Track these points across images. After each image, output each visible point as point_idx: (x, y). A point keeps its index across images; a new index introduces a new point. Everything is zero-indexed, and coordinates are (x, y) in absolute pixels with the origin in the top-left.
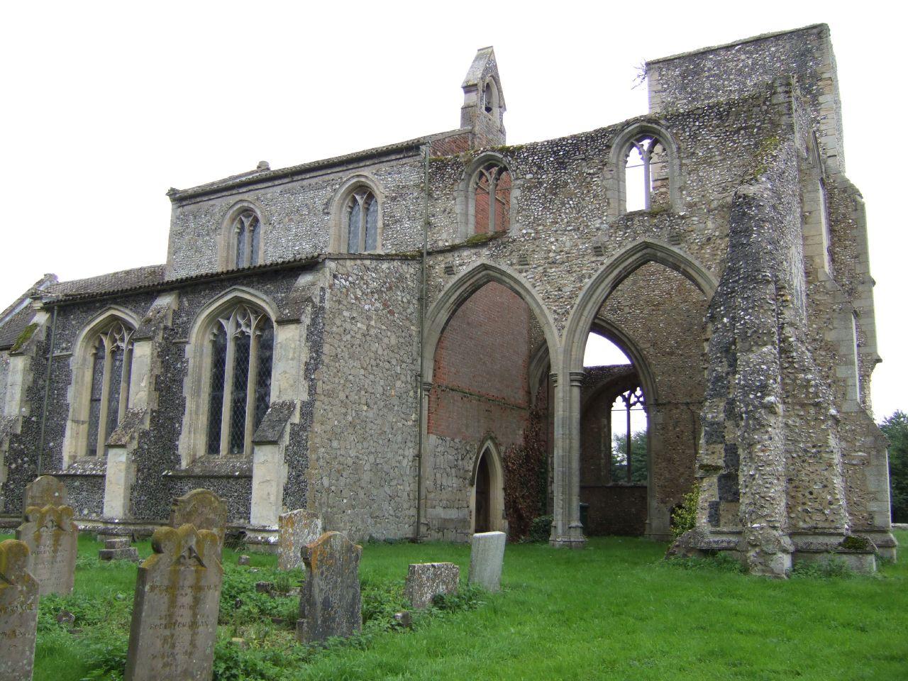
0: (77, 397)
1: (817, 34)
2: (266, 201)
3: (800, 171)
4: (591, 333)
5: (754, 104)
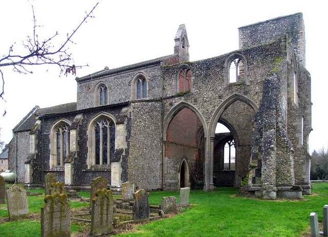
0: (53, 147)
1: (299, 16)
2: (109, 81)
3: (288, 69)
4: (218, 123)
5: (273, 44)
